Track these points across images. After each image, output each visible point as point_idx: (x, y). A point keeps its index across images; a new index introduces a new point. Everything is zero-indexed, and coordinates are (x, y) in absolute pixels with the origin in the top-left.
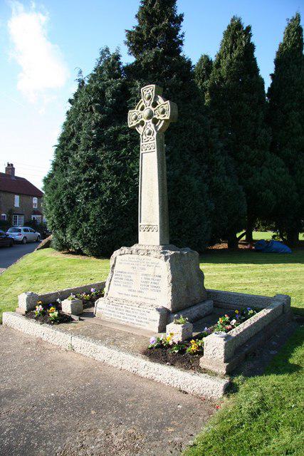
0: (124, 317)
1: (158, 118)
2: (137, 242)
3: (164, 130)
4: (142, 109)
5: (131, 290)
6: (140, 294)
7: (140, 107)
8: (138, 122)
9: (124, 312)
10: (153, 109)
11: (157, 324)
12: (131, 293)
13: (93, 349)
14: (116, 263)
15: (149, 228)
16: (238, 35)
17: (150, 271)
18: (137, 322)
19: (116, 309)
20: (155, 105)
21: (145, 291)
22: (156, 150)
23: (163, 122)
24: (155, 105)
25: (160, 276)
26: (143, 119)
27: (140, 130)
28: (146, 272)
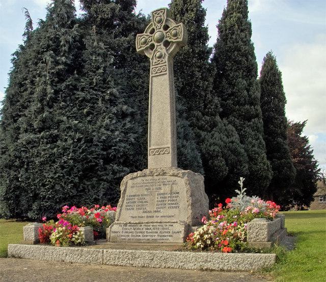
0: (144, 236)
1: (170, 40)
2: (146, 167)
3: (174, 54)
4: (153, 32)
5: (145, 212)
6: (157, 214)
7: (150, 30)
8: (148, 45)
9: (144, 230)
10: (164, 32)
11: (182, 235)
12: (145, 215)
13: (130, 256)
14: (128, 189)
15: (160, 151)
16: (149, 15)
17: (166, 189)
18: (159, 238)
19: (134, 229)
20: (166, 27)
21: (162, 210)
22: (167, 72)
23: (174, 45)
24: (166, 27)
25: (178, 193)
26: (153, 42)
27: (149, 55)
28: (162, 191)
